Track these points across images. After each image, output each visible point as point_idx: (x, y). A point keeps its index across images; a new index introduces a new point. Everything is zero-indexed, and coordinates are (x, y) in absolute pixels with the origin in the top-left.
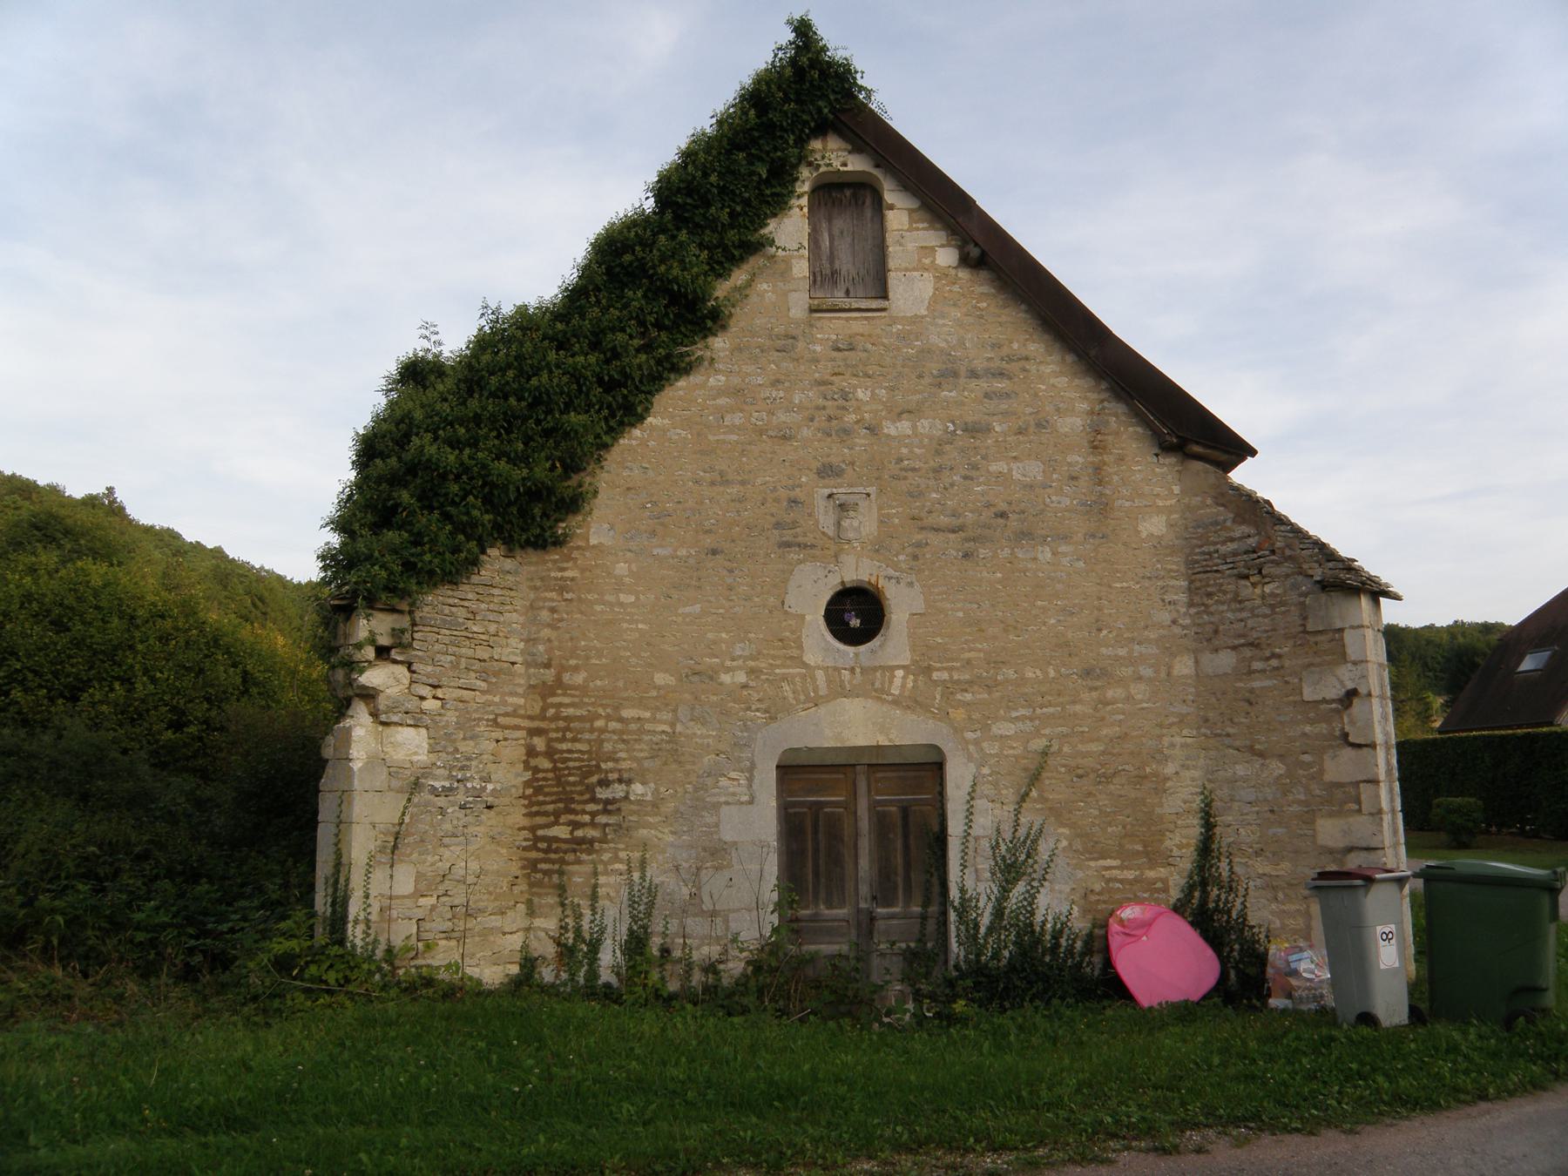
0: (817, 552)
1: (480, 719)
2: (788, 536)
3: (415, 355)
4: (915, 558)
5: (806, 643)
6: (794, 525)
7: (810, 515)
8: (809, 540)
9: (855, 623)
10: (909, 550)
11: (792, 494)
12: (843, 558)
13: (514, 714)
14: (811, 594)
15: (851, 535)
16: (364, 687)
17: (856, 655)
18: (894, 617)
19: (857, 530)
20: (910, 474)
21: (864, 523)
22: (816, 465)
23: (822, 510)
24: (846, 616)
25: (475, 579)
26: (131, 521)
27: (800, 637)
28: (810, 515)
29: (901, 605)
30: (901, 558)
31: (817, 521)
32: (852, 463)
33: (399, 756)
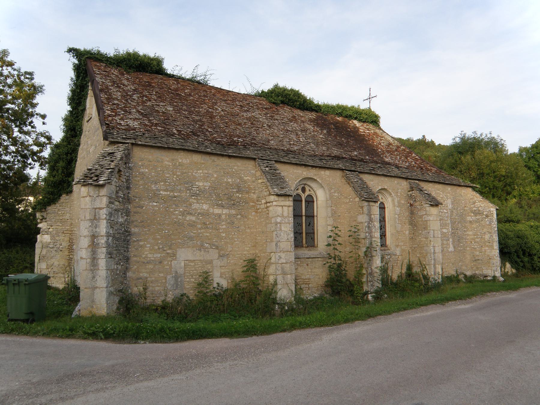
3: (106, 54)
13: (67, 230)
16: (8, 62)
25: (59, 202)
26: (178, 79)
33: (45, 241)
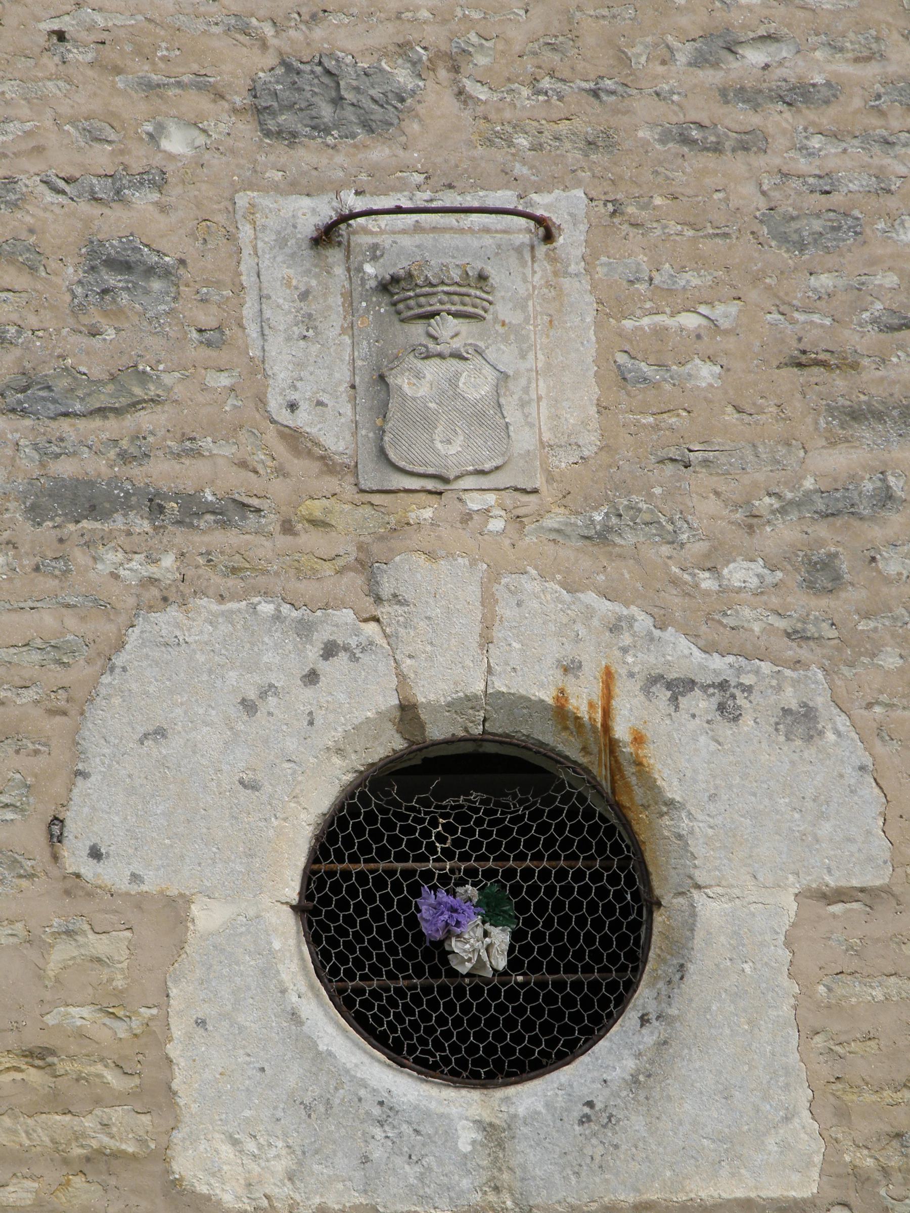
0: (259, 544)
1: (45, 209)
2: (87, 452)
4: (822, 574)
5: (196, 1066)
6: (127, 392)
7: (213, 338)
8: (212, 474)
9: (482, 946)
10: (783, 534)
11: (113, 224)
12: (408, 573)
14: (224, 771)
15: (451, 449)
17: (495, 1135)
18: (710, 910)
19: (488, 418)
20: (777, 120)
21: (529, 384)
22: (244, 65)
23: (282, 311)
24: (429, 908)
27: (155, 1035)
28: (213, 338)
29: (746, 840)
30: (741, 573)
31: (258, 369)
32: (455, 61)
